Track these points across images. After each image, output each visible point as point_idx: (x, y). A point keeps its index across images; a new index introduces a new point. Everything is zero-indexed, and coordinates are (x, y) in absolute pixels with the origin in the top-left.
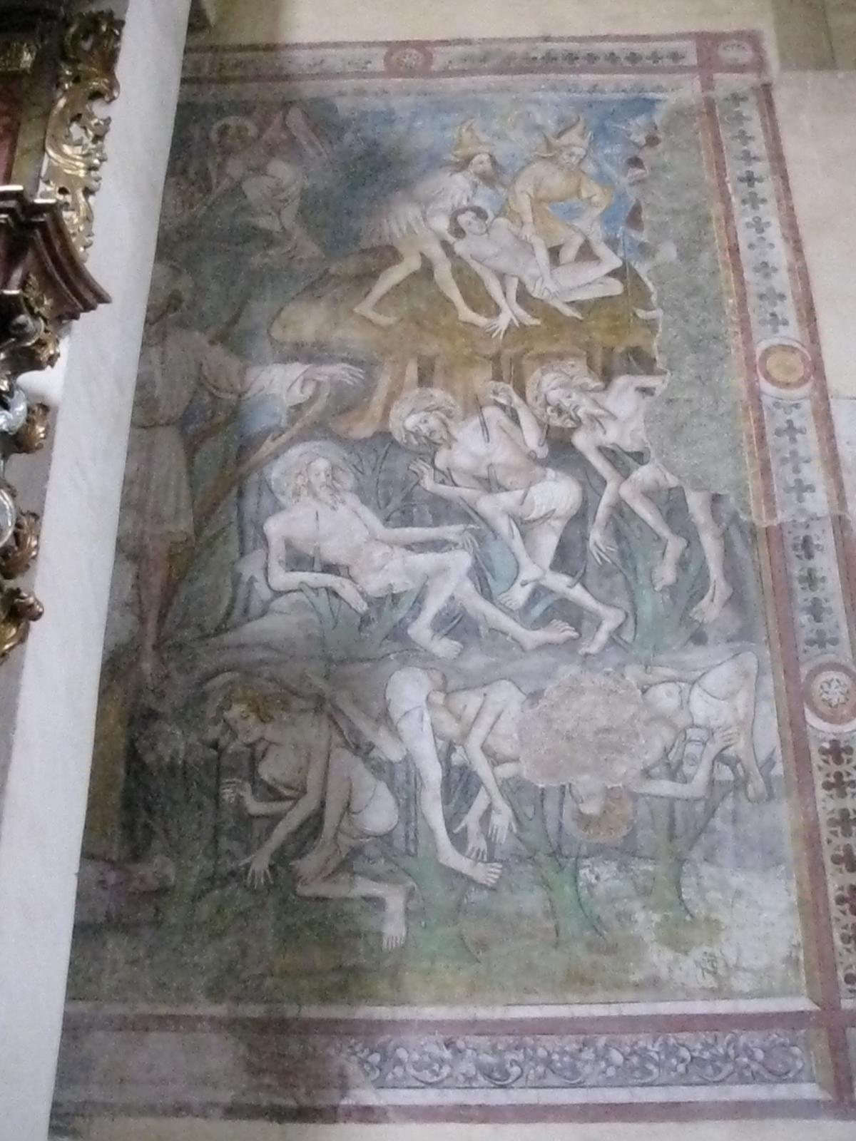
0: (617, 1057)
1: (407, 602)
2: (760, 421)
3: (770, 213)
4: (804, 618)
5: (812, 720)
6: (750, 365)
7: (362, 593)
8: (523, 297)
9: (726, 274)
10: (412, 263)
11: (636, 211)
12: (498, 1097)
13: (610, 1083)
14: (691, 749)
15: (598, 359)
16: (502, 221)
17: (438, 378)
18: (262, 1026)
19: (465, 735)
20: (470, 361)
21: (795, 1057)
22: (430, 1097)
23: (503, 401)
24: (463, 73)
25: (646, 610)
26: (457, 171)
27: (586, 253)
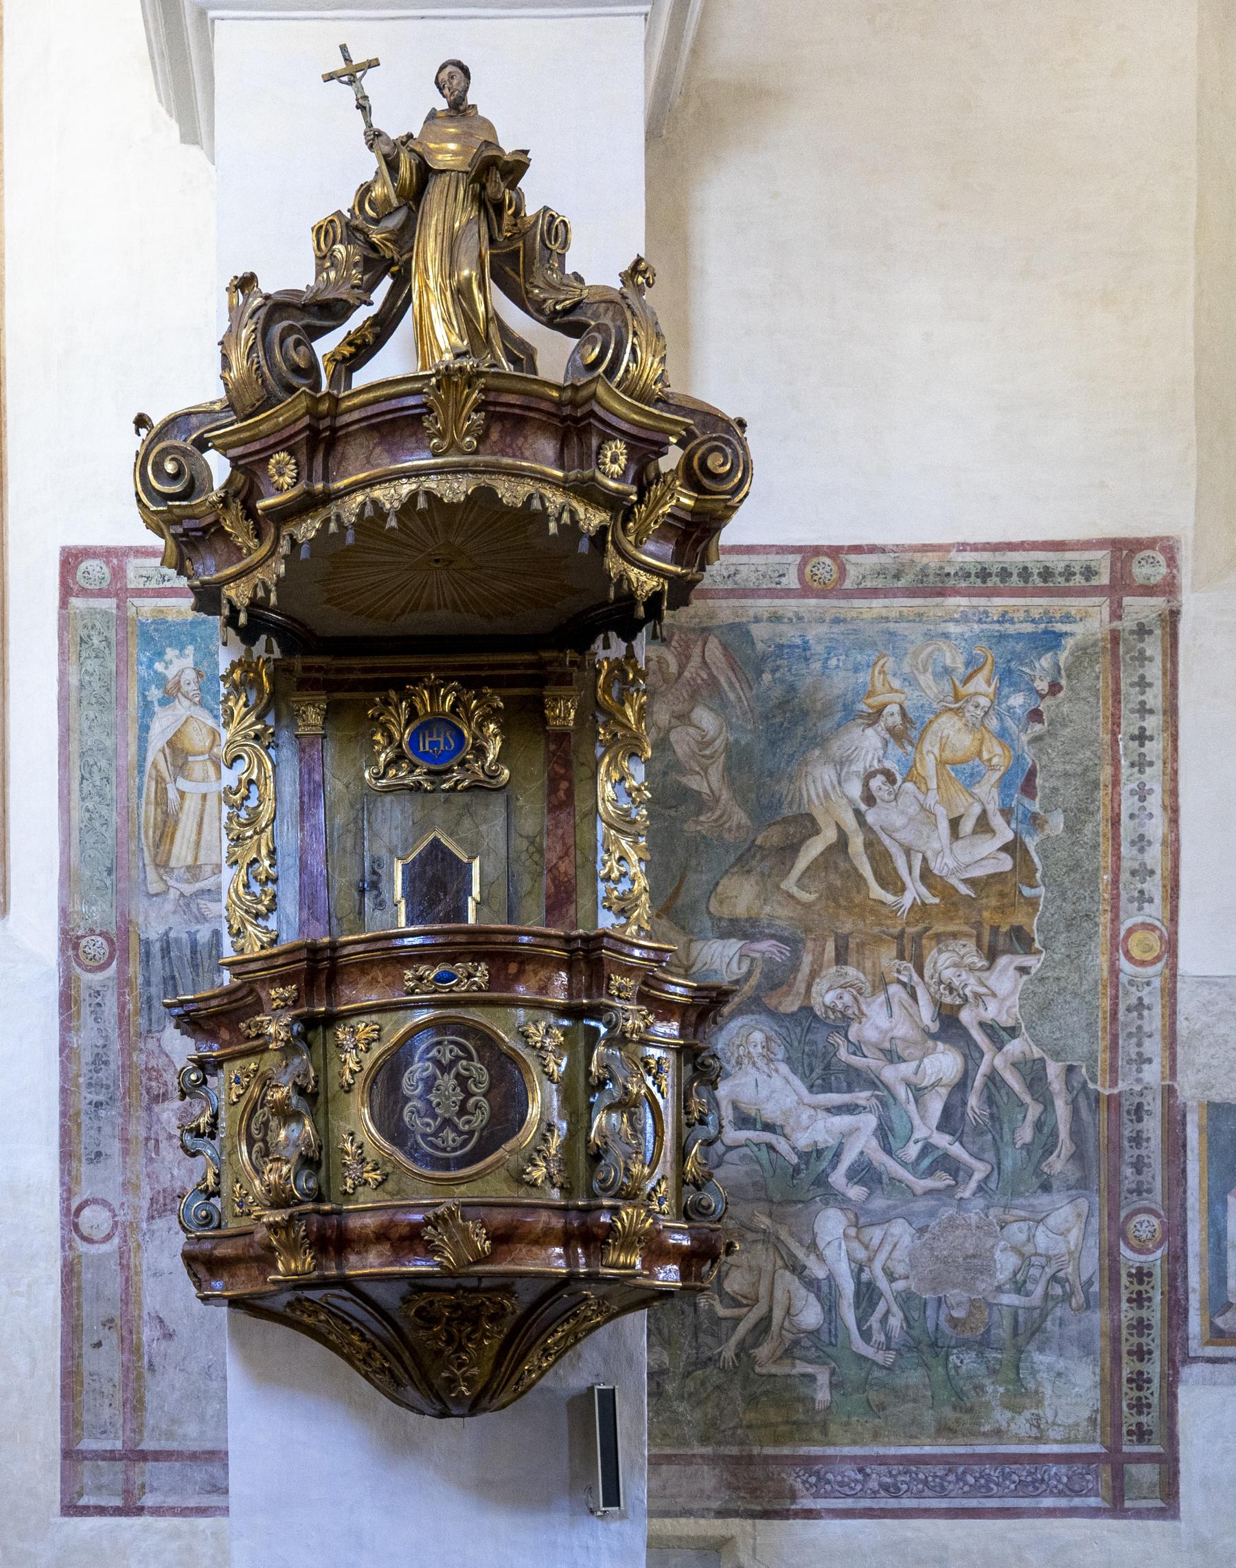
0: (971, 1480)
1: (828, 1155)
2: (1115, 997)
3: (1154, 778)
4: (1128, 1171)
5: (1125, 1251)
6: (1116, 944)
7: (794, 1149)
8: (926, 876)
9: (1106, 846)
10: (829, 835)
11: (1032, 774)
12: (893, 1503)
13: (965, 1495)
14: (1033, 1271)
15: (986, 938)
16: (909, 786)
17: (853, 957)
18: (736, 1460)
19: (871, 1260)
20: (878, 940)
21: (1088, 1481)
22: (849, 1503)
23: (905, 979)
24: (874, 593)
25: (1008, 1164)
26: (870, 725)
27: (983, 826)
